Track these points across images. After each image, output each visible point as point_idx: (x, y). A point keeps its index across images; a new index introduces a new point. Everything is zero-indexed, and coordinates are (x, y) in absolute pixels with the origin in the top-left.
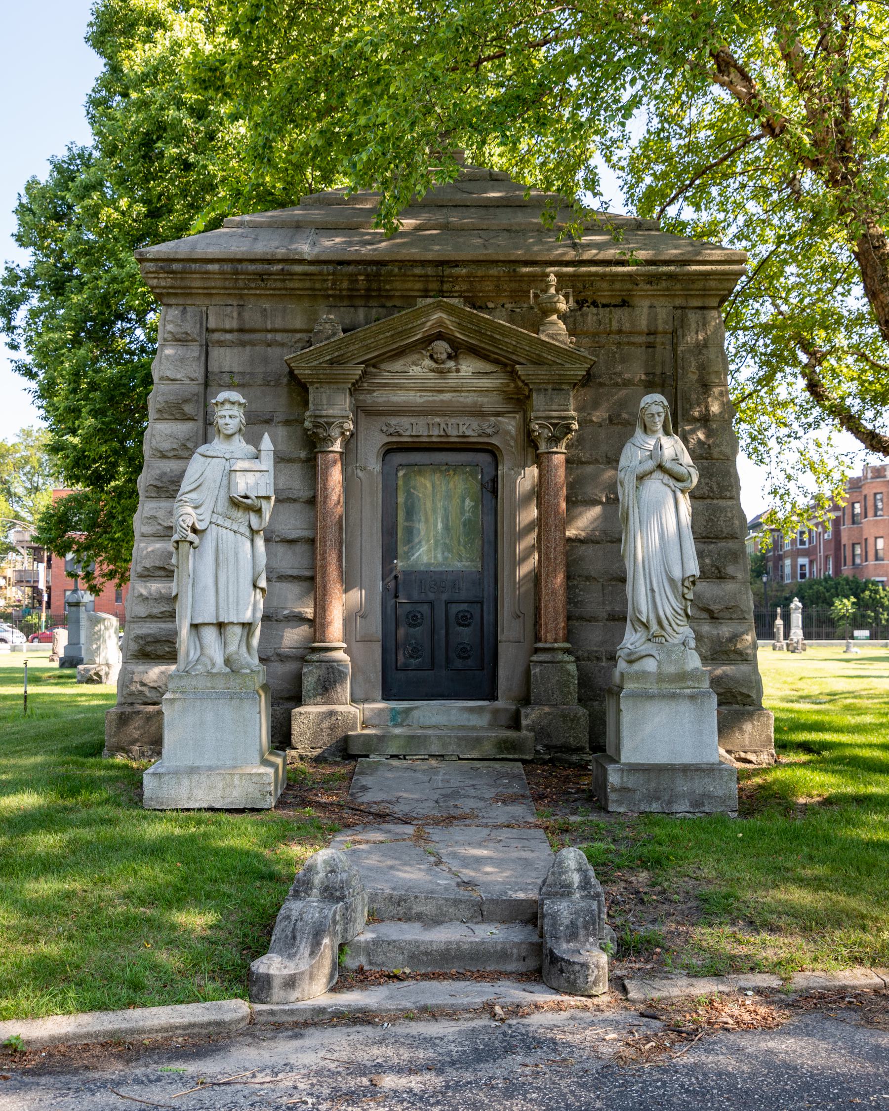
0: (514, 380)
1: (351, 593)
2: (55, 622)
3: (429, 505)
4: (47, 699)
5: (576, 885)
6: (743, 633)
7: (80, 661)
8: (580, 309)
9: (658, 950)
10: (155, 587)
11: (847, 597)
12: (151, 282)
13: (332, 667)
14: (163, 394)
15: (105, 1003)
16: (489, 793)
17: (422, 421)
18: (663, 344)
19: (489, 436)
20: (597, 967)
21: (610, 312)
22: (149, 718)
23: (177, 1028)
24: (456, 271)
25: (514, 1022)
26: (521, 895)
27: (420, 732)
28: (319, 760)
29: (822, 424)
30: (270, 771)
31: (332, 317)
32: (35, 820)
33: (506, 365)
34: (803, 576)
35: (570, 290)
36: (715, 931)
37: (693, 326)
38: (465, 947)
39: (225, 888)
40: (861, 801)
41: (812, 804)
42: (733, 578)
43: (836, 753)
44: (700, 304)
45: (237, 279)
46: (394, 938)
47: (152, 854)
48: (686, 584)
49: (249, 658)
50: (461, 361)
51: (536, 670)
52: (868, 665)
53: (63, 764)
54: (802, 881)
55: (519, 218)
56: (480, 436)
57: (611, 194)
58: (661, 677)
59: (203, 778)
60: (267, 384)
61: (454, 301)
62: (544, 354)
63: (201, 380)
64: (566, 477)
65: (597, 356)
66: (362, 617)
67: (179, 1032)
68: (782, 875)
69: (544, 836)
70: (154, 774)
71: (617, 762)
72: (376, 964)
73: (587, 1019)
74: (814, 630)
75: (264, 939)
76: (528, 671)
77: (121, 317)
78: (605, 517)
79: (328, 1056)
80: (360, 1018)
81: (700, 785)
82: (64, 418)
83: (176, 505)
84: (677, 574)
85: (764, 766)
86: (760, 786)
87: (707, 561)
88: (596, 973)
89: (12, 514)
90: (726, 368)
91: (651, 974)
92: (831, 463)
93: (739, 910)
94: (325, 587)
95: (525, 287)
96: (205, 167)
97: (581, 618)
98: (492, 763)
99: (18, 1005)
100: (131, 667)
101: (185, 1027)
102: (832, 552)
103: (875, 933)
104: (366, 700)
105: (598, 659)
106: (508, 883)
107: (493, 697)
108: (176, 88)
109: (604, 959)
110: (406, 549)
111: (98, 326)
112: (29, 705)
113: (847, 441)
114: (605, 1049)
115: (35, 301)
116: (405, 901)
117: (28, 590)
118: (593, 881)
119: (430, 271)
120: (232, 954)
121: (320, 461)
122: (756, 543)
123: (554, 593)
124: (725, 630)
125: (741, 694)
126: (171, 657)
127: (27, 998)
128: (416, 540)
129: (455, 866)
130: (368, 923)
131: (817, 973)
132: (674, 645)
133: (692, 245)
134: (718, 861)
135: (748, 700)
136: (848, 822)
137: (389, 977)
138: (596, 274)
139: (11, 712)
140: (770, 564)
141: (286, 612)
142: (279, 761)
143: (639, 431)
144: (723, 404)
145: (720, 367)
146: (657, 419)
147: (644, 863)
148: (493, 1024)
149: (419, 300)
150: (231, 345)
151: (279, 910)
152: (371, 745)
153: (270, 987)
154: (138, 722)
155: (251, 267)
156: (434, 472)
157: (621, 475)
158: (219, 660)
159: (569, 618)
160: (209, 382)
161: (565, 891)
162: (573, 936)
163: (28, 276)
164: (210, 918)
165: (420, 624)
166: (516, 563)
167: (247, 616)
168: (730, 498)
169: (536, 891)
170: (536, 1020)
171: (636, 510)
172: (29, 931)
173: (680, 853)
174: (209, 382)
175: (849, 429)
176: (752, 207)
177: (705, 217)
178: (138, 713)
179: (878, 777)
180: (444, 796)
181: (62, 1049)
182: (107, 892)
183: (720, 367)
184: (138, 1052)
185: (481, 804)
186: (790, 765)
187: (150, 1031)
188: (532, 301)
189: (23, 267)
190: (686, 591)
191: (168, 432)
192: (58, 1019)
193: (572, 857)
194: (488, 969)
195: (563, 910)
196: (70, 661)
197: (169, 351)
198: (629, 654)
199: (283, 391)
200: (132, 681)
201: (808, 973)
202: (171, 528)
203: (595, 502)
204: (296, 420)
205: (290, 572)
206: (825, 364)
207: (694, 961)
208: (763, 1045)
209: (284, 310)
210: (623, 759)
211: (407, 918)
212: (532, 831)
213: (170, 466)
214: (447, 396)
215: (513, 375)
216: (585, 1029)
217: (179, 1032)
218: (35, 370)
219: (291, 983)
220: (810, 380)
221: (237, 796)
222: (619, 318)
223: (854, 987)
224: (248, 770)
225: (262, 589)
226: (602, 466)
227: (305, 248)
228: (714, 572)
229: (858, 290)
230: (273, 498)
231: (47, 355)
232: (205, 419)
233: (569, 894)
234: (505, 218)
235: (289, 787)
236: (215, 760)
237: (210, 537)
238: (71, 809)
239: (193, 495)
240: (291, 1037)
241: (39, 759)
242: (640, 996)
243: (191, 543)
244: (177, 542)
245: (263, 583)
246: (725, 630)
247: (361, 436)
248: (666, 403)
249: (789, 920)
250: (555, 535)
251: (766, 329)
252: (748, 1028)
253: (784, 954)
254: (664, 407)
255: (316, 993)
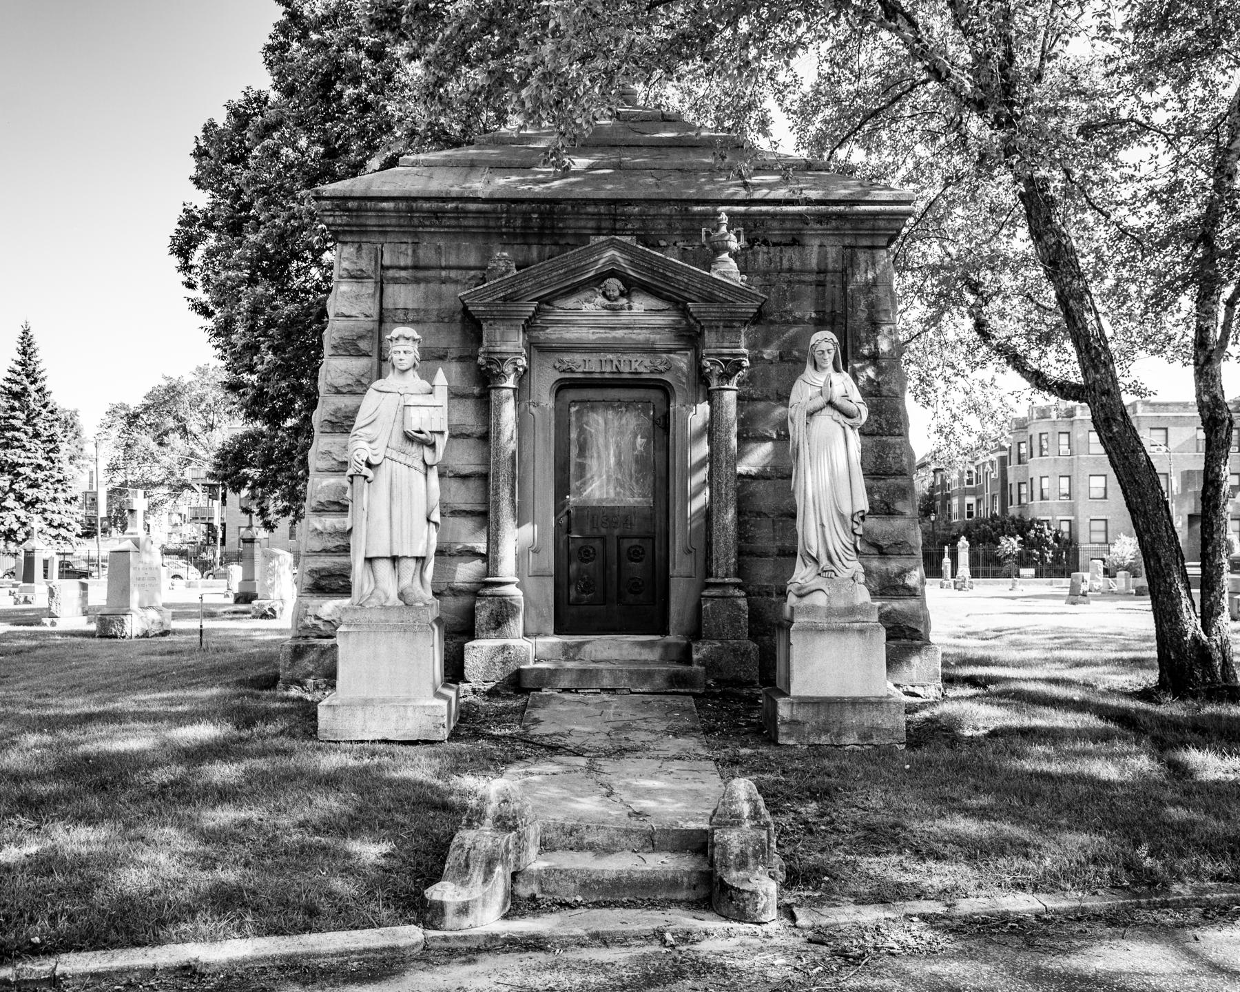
0: (685, 318)
1: (523, 528)
2: (227, 559)
3: (601, 440)
4: (221, 633)
5: (746, 815)
6: (911, 569)
7: (255, 597)
8: (751, 248)
9: (826, 878)
10: (331, 522)
11: (1013, 536)
12: (326, 220)
13: (505, 601)
14: (338, 330)
15: (281, 928)
16: (661, 726)
17: (594, 358)
18: (833, 282)
19: (661, 372)
20: (766, 895)
21: (781, 251)
22: (324, 652)
23: (352, 952)
24: (628, 209)
25: (684, 948)
26: (692, 825)
27: (592, 666)
28: (492, 694)
29: (989, 364)
30: (444, 703)
31: (505, 254)
32: (211, 750)
33: (677, 303)
34: (970, 515)
35: (741, 229)
36: (883, 860)
37: (863, 266)
38: (637, 875)
39: (399, 818)
40: (1029, 734)
41: (978, 737)
42: (902, 514)
43: (1002, 687)
44: (869, 243)
45: (411, 217)
46: (566, 867)
47: (327, 784)
48: (856, 519)
49: (422, 592)
50: (633, 299)
51: (707, 605)
52: (1033, 602)
53: (238, 696)
54: (967, 810)
55: (692, 158)
57: (783, 138)
58: (830, 612)
59: (377, 710)
60: (440, 320)
61: (627, 239)
62: (714, 293)
63: (376, 317)
64: (737, 414)
65: (768, 294)
66: (534, 552)
67: (354, 956)
68: (951, 806)
69: (714, 768)
70: (329, 706)
71: (787, 695)
72: (548, 892)
73: (758, 941)
74: (981, 568)
75: (438, 867)
76: (699, 606)
77: (296, 256)
78: (776, 454)
79: (501, 980)
80: (534, 944)
81: (868, 718)
82: (241, 358)
83: (351, 440)
84: (847, 511)
85: (931, 699)
86: (927, 720)
87: (877, 497)
88: (765, 900)
89: (188, 452)
90: (894, 307)
91: (819, 902)
92: (996, 405)
93: (905, 839)
94: (498, 522)
95: (696, 225)
96: (384, 107)
97: (751, 553)
98: (663, 697)
99: (196, 929)
100: (306, 601)
101: (360, 952)
102: (998, 492)
103: (1037, 859)
104: (538, 634)
105: (769, 594)
106: (679, 814)
107: (664, 631)
108: (354, 31)
109: (773, 887)
110: (578, 484)
111: (272, 267)
112: (204, 640)
113: (1013, 380)
114: (774, 974)
115: (212, 241)
116: (577, 831)
117: (204, 528)
118: (763, 811)
119: (603, 209)
120: (405, 882)
121: (493, 397)
122: (922, 483)
123: (725, 528)
124: (894, 566)
125: (910, 628)
126: (346, 591)
127: (205, 922)
128: (588, 476)
129: (626, 796)
130: (540, 853)
131: (981, 899)
132: (844, 580)
133: (861, 185)
134: (886, 791)
135: (916, 635)
136: (1012, 753)
137: (561, 904)
138: (767, 213)
139: (186, 646)
140: (938, 503)
141: (459, 547)
142: (452, 694)
143: (809, 368)
144: (892, 342)
145: (889, 306)
146: (827, 356)
147: (814, 794)
148: (664, 950)
149: (592, 238)
150: (405, 282)
151: (451, 839)
152: (544, 679)
153: (443, 914)
154: (313, 656)
155: (426, 205)
156: (607, 408)
157: (791, 411)
158: (393, 594)
159: (740, 553)
160: (383, 318)
161: (735, 821)
162: (742, 864)
163: (206, 217)
164: (385, 848)
165: (593, 559)
166: (687, 499)
167: (420, 552)
168: (900, 435)
169: (707, 820)
170: (706, 947)
171: (807, 446)
172: (206, 858)
173: (849, 784)
174: (383, 318)
175: (1016, 368)
176: (920, 149)
177: (874, 160)
178: (313, 646)
179: (1045, 711)
180: (616, 729)
181: (240, 972)
182: (284, 821)
183: (889, 306)
184: (314, 975)
185: (652, 737)
186: (957, 699)
187: (325, 956)
188: (704, 239)
189: (200, 208)
190: (855, 526)
191: (343, 368)
192: (237, 942)
193: (743, 787)
194: (659, 897)
195: (733, 839)
196: (245, 597)
197: (344, 288)
198: (799, 589)
199: (457, 327)
200: (306, 615)
201: (972, 899)
202: (346, 463)
203: (765, 439)
204: (470, 357)
205: (463, 507)
206: (991, 304)
207: (861, 889)
208: (928, 969)
209: (459, 247)
210: (793, 693)
211: (580, 847)
212: (702, 763)
213: (345, 402)
214: (619, 334)
215: (685, 312)
216: (753, 954)
217: (354, 956)
218: (211, 308)
219: (464, 910)
220: (977, 320)
221: (410, 729)
222: (790, 257)
223: (1017, 913)
224: (421, 703)
225: (436, 523)
227: (480, 185)
228: (883, 508)
229: (1023, 232)
230: (447, 434)
231: (225, 294)
232: (380, 355)
233: (739, 824)
234: (676, 158)
235: (462, 720)
236: (388, 694)
237: (384, 472)
238: (247, 740)
239: (367, 430)
240: (464, 963)
241: (215, 691)
242: (810, 924)
243: (366, 477)
244: (352, 476)
245: (436, 517)
246: (894, 566)
247: (534, 373)
248: (836, 341)
249: (955, 848)
250: (725, 470)
251: (935, 270)
252: (914, 954)
253: (949, 882)
254: (834, 344)
255: (488, 919)
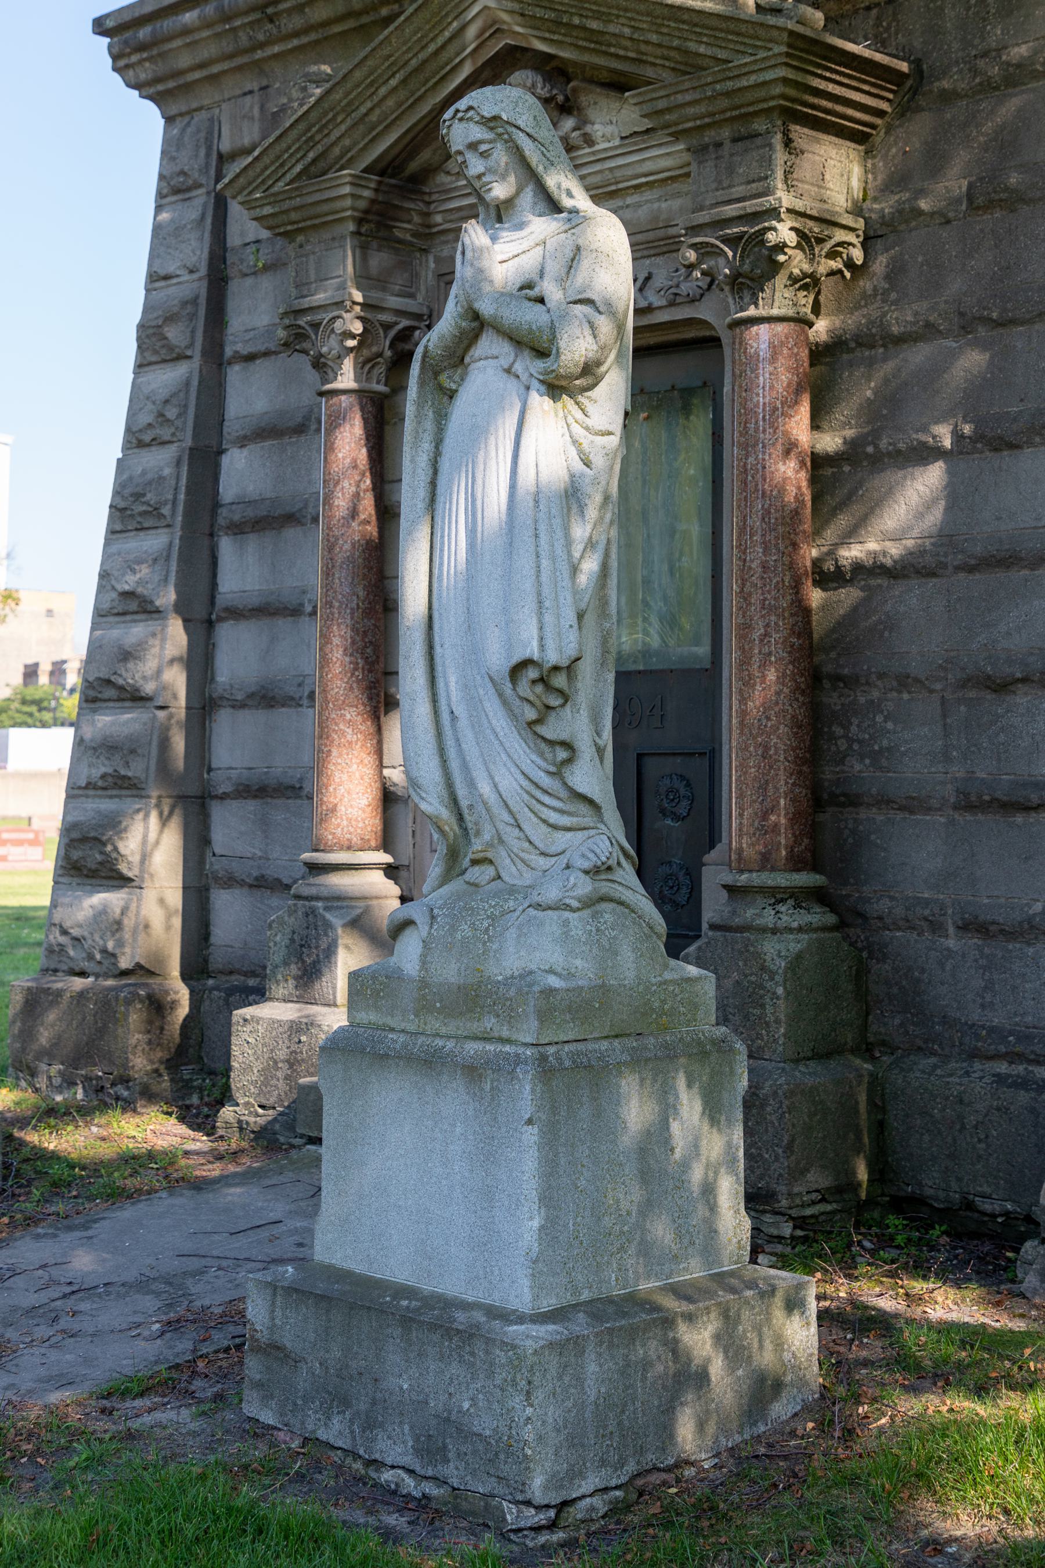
56: (672, 304)
105: (936, 927)
226: (950, 343)
